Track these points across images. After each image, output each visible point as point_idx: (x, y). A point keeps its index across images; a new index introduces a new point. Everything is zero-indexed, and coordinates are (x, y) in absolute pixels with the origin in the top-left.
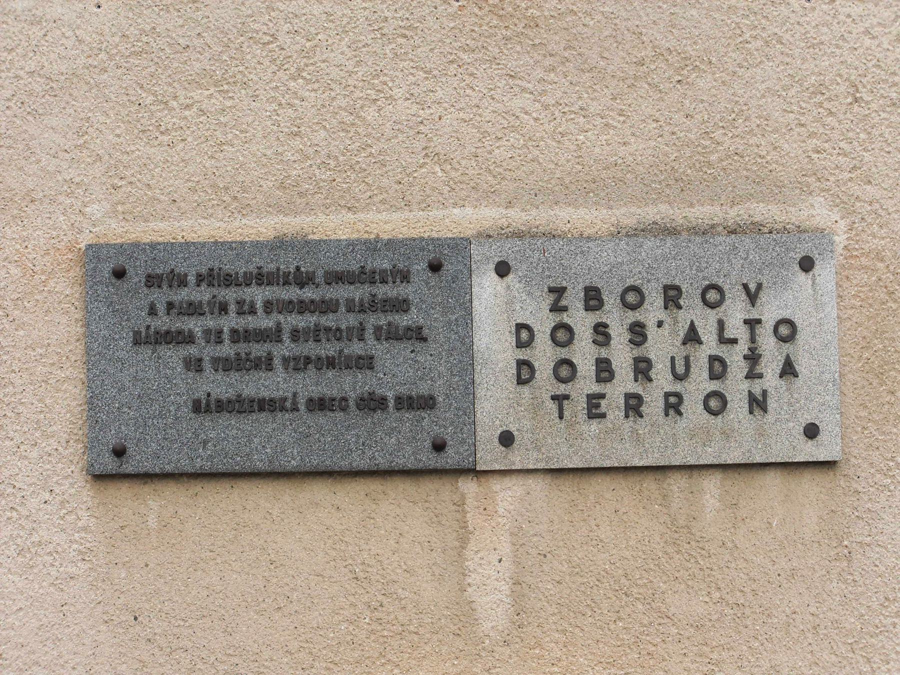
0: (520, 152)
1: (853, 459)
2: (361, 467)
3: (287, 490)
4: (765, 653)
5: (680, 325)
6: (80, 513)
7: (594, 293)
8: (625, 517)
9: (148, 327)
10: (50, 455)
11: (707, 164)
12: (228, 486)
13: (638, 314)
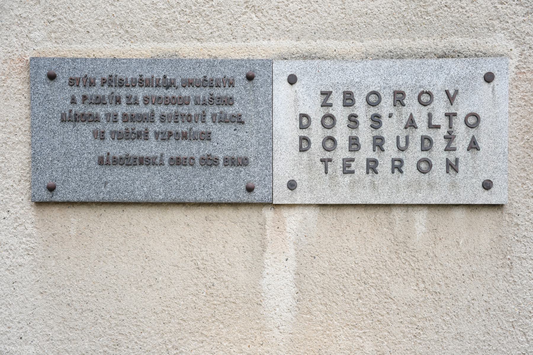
0: (306, 5)
1: (515, 204)
2: (202, 201)
3: (157, 214)
4: (453, 324)
5: (403, 116)
6: (27, 225)
7: (349, 95)
8: (365, 235)
9: (71, 111)
10: (8, 189)
11: (425, 13)
12: (121, 210)
13: (377, 109)
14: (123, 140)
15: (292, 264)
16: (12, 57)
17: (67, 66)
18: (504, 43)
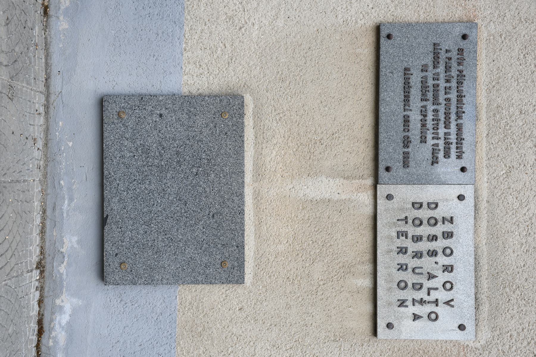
1: (376, 344)
8: (355, 245)
9: (441, 49)
14: (421, 84)
15: (336, 197)
16: (477, 11)
17: (471, 47)
18: (484, 337)
